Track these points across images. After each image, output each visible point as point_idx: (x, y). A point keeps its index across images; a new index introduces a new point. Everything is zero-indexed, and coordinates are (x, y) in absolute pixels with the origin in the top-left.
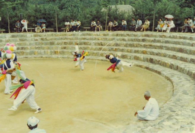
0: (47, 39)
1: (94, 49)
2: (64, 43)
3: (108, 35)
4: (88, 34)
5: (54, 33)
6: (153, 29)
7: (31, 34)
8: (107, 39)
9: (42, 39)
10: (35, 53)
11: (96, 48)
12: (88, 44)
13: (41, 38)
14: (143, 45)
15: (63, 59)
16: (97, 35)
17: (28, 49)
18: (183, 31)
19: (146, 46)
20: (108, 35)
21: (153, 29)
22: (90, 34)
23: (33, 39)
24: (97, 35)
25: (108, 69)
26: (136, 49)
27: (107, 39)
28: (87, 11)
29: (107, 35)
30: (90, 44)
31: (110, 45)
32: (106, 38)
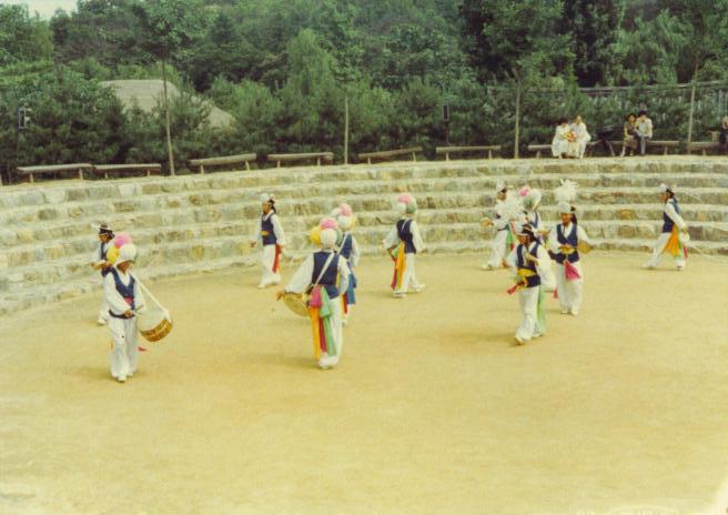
0: (214, 198)
1: (428, 219)
2: (292, 207)
3: (409, 174)
4: (335, 175)
5: (159, 180)
6: (517, 151)
7: (132, 186)
8: (429, 188)
9: (194, 201)
10: (243, 248)
11: (435, 217)
12: (382, 207)
13: (190, 197)
14: (588, 196)
15: (366, 258)
16: (371, 177)
17: (193, 236)
18: (624, 153)
19: (601, 197)
20: (409, 174)
21: (517, 151)
22: (343, 175)
23: (163, 202)
24: (371, 177)
25: (346, 311)
26: (707, 190)
27: (429, 188)
28: (640, 72)
29: (406, 174)
30: (386, 205)
31: (464, 205)
32: (424, 185)
